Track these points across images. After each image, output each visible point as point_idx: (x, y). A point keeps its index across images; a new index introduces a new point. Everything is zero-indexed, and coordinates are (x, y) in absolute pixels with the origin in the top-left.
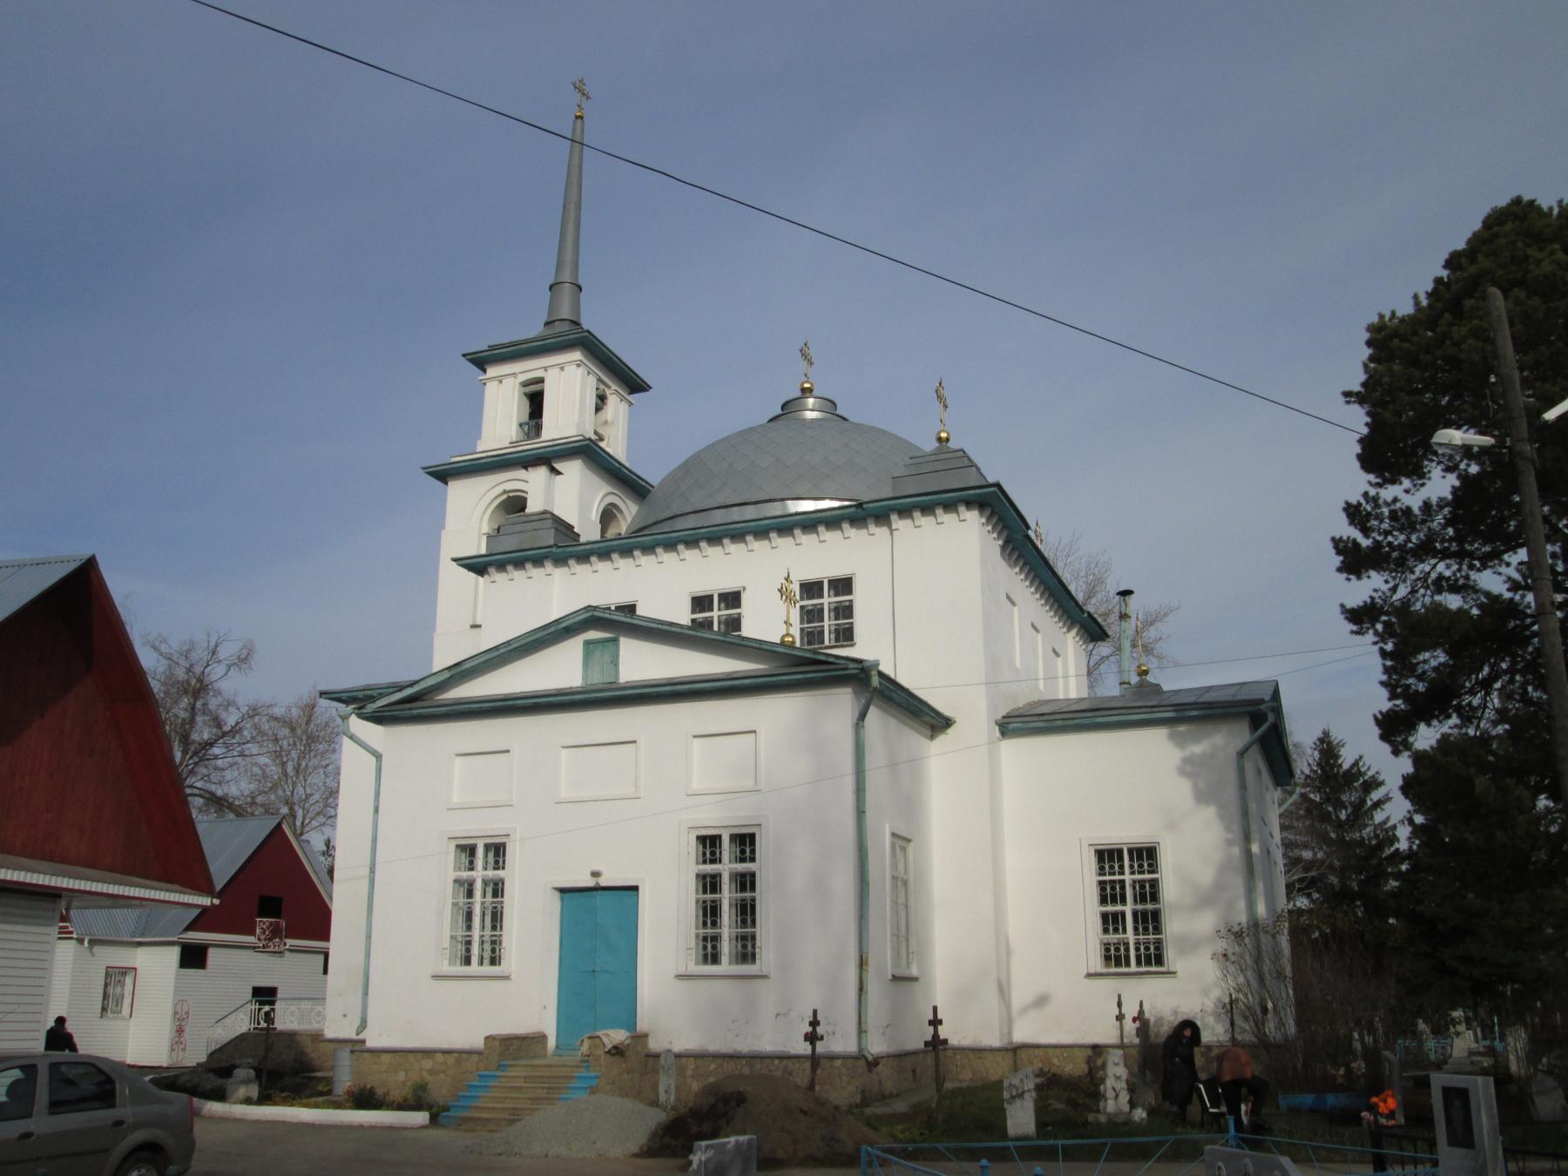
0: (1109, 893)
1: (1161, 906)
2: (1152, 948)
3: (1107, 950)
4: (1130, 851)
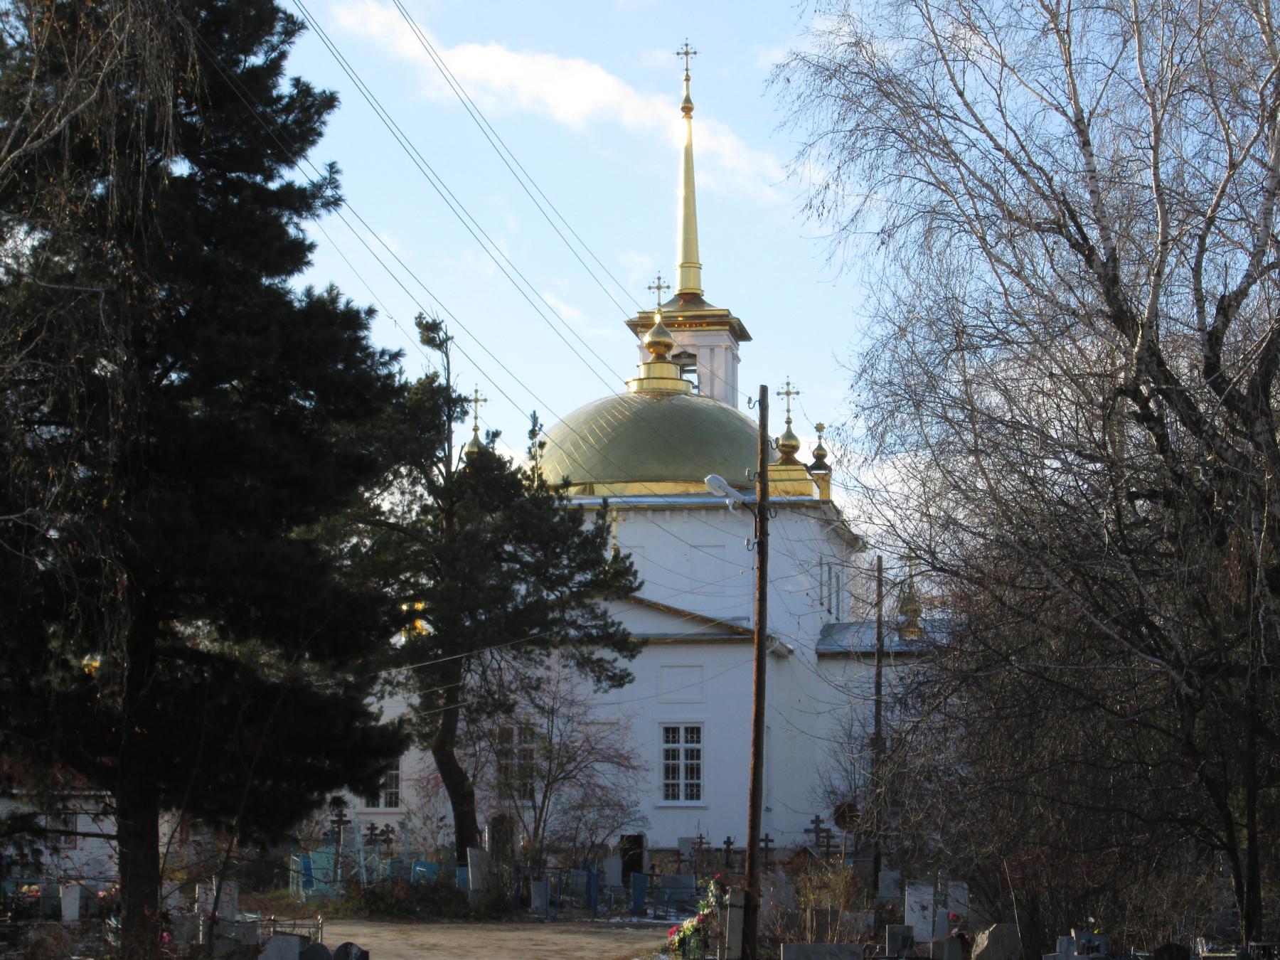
4: (686, 729)
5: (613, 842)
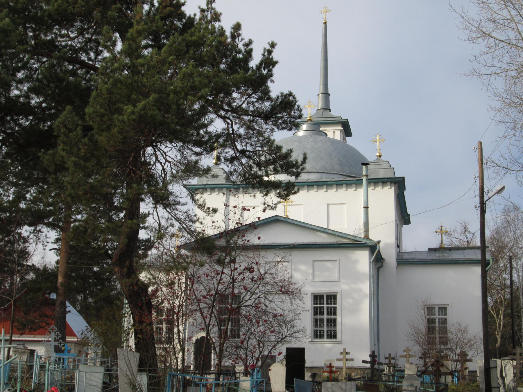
0: (332, 322)
2: (333, 332)
3: (334, 302)
4: (327, 296)
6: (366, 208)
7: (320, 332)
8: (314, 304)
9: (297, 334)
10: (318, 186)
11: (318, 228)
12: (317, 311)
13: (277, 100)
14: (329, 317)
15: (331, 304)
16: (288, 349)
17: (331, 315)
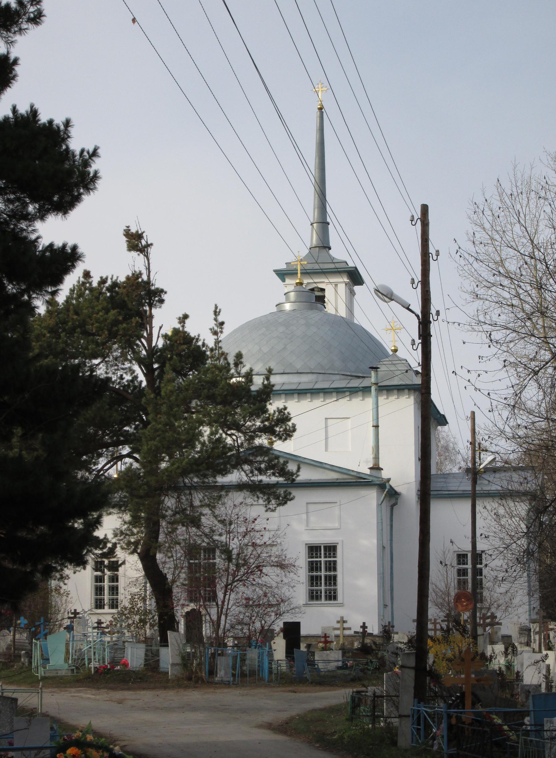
0: (332, 580)
1: (323, 601)
3: (334, 554)
4: (325, 547)
5: (278, 626)
6: (377, 427)
7: (317, 593)
8: (309, 558)
9: (293, 611)
10: (312, 393)
11: (312, 463)
12: (313, 567)
13: (274, 414)
14: (328, 573)
15: (330, 557)
16: (285, 624)
17: (330, 570)
